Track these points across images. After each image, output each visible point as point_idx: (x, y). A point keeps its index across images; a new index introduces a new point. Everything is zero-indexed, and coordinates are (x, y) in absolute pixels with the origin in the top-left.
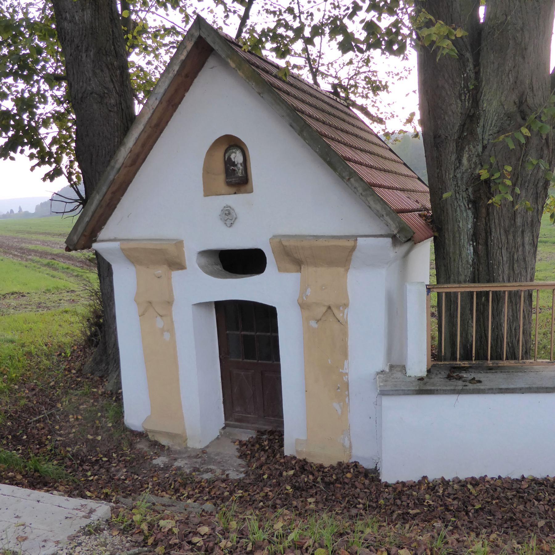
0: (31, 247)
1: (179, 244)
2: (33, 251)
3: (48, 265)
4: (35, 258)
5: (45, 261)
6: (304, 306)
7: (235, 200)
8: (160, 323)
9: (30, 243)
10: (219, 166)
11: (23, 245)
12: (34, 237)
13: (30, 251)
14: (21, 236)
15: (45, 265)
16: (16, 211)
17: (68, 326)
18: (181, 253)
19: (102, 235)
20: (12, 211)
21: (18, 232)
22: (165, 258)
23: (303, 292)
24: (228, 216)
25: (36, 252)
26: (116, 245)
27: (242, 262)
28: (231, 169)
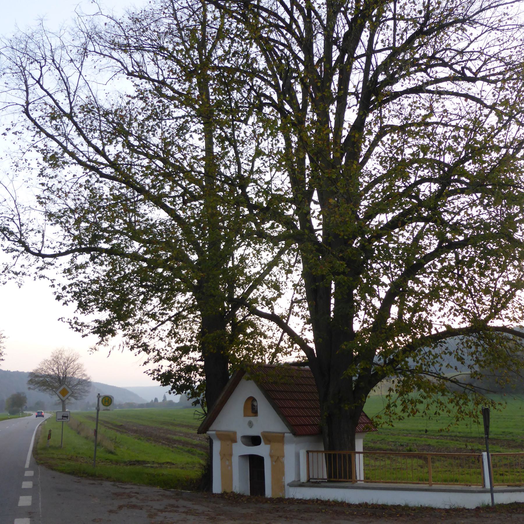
0: (175, 437)
1: (235, 433)
2: (177, 441)
3: (188, 451)
4: (179, 446)
5: (187, 449)
6: (271, 456)
7: (252, 419)
8: (227, 463)
9: (175, 435)
10: (250, 406)
11: (169, 436)
12: (178, 429)
13: (175, 441)
14: (166, 427)
15: (186, 452)
16: (160, 400)
17: (195, 473)
18: (235, 437)
19: (211, 428)
20: (156, 399)
21: (164, 423)
22: (229, 438)
23: (271, 451)
24: (250, 424)
25: (179, 442)
26: (214, 432)
27: (255, 441)
28: (252, 409)
